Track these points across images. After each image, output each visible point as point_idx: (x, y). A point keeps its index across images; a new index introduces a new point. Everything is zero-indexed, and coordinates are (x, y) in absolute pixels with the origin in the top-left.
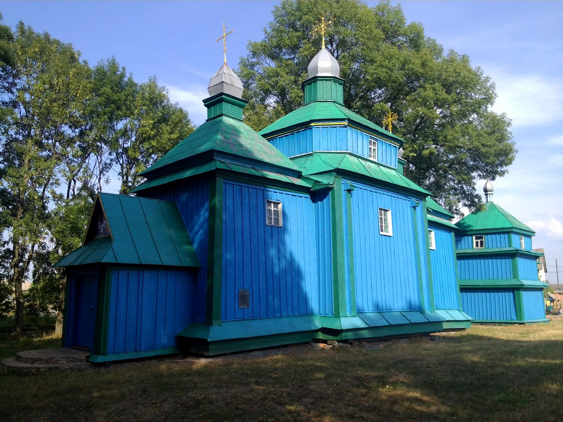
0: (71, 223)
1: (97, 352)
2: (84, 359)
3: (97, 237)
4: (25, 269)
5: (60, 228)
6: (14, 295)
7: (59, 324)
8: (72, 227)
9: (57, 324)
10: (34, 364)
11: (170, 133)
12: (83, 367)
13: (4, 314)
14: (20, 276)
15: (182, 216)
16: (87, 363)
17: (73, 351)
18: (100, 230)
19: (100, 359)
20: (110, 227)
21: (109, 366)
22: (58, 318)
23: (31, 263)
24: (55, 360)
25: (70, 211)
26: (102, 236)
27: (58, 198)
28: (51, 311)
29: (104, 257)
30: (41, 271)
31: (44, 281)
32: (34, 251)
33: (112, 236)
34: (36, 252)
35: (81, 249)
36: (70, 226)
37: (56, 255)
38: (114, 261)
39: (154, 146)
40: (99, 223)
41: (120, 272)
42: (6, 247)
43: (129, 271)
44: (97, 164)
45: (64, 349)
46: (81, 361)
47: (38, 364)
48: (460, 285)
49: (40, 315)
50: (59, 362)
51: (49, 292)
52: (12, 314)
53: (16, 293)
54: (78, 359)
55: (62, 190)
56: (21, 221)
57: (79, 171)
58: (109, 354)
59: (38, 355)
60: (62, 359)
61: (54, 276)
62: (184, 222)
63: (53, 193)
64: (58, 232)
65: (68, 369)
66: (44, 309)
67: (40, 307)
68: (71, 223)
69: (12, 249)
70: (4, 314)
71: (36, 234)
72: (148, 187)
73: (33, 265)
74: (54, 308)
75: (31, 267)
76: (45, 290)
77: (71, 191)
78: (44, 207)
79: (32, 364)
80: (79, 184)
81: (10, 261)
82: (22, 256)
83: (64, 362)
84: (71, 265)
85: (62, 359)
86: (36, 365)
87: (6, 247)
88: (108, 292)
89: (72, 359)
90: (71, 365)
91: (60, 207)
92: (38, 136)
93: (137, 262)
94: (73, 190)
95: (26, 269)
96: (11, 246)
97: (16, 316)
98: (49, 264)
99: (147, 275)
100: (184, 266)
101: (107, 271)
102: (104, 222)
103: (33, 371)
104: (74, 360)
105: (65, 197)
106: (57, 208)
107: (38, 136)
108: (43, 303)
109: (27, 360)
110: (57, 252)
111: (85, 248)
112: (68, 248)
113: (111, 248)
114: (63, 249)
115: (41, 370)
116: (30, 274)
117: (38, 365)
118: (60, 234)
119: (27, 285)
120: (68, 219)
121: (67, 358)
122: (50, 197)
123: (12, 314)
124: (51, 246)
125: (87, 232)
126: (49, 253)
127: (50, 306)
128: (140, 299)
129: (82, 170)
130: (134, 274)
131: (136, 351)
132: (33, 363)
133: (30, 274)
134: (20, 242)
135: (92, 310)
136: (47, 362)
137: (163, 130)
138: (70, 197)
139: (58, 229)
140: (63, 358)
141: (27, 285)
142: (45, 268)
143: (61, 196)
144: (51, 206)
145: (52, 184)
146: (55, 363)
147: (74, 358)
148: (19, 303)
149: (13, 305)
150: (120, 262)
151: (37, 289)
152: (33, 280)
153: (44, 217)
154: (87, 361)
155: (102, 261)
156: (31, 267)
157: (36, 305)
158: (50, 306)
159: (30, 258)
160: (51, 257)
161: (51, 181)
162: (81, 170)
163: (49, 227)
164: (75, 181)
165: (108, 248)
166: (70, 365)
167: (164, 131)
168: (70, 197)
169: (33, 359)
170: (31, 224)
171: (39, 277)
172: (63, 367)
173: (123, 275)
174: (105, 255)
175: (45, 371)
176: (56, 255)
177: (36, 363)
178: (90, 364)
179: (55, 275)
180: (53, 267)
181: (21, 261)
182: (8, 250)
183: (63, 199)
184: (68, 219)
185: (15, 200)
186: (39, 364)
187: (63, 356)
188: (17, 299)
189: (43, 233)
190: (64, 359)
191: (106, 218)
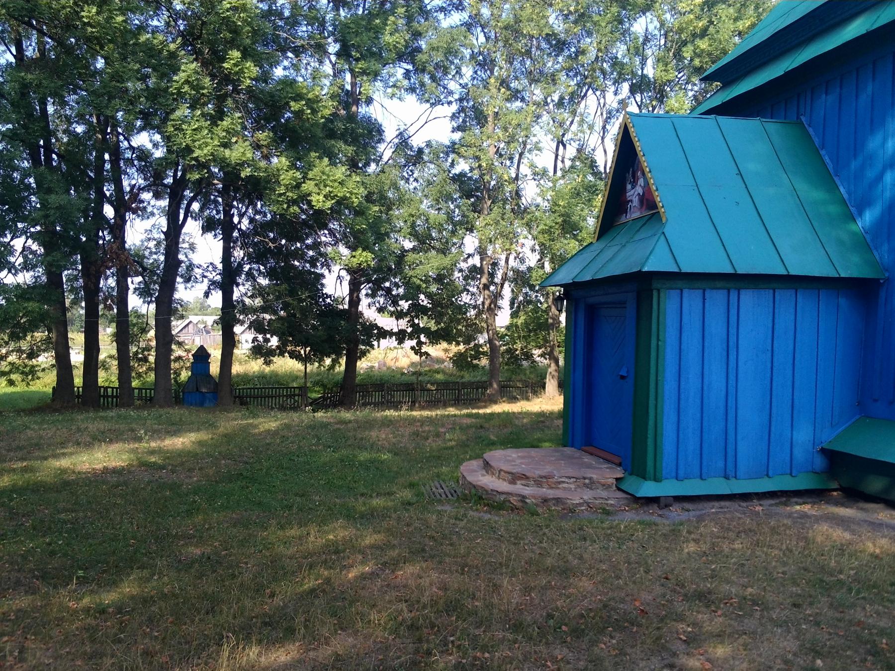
0: (562, 215)
1: (643, 475)
2: (613, 484)
3: (623, 219)
4: (498, 295)
5: (545, 225)
6: (486, 335)
7: (552, 381)
8: (564, 221)
9: (547, 380)
10: (515, 483)
11: (736, 20)
12: (612, 502)
13: (475, 362)
14: (493, 308)
15: (823, 152)
16: (620, 495)
17: (587, 459)
18: (631, 201)
19: (648, 489)
20: (657, 190)
21: (667, 506)
22: (550, 370)
23: (506, 285)
24: (554, 480)
25: (559, 195)
26: (636, 215)
27: (539, 174)
28: (538, 359)
29: (648, 258)
30: (521, 298)
31: (526, 313)
32: (510, 267)
33: (663, 210)
34: (513, 269)
35: (592, 248)
36: (560, 220)
37: (541, 272)
38: (673, 268)
39: (703, 51)
40: (629, 187)
41: (708, 294)
42: (471, 262)
43: (704, 291)
44: (599, 108)
45: (568, 450)
46: (607, 487)
47: (522, 485)
48: (625, 308)
49: (522, 365)
50: (560, 486)
51: (535, 330)
52: (484, 362)
53: (488, 333)
54: (598, 482)
55: (545, 160)
56: (488, 218)
57: (572, 123)
58: (666, 479)
59: (522, 463)
60: (567, 480)
61: (539, 305)
62: (830, 167)
63: (532, 166)
64: (543, 232)
65: (580, 505)
66: (528, 356)
67: (523, 354)
68: (562, 215)
69: (479, 265)
70: (475, 362)
71: (511, 238)
72: (728, 99)
73: (510, 289)
74: (542, 355)
75: (507, 292)
76: (527, 328)
77: (560, 165)
78: (518, 194)
79: (511, 483)
80: (571, 151)
81: (477, 283)
82: (492, 275)
83: (572, 486)
84: (576, 280)
85: (567, 480)
86: (519, 488)
87: (471, 262)
88: (658, 340)
89: (587, 481)
90: (588, 495)
91: (544, 189)
92: (500, 58)
93: (728, 270)
94: (563, 161)
95: (500, 295)
96: (476, 261)
97: (490, 365)
98: (532, 287)
99: (748, 298)
100: (843, 275)
101: (655, 294)
102: (641, 182)
103: (513, 499)
104: (591, 485)
105: (551, 173)
106: (539, 192)
107: (500, 58)
108: (526, 347)
109: (502, 473)
110: (543, 267)
111: (598, 246)
112: (560, 261)
113: (662, 238)
114: (552, 261)
115: (528, 501)
116: (505, 303)
117: (522, 487)
118: (546, 236)
119: (503, 319)
120: (557, 208)
121: (577, 478)
122: (529, 175)
123: (484, 362)
124: (532, 259)
125: (601, 217)
126: (530, 269)
127: (536, 352)
128: (732, 357)
129: (577, 119)
130: (717, 298)
131: (727, 477)
132: (513, 482)
133: (505, 303)
134: (489, 253)
135: (623, 377)
136: (538, 483)
137: (721, 17)
138: (559, 173)
139: (541, 227)
140: (570, 478)
141: (503, 319)
142: (526, 293)
143: (545, 172)
144: (530, 192)
145: (530, 151)
146: (553, 486)
147: (590, 479)
148: (493, 348)
149: (486, 349)
150: (685, 269)
151: (517, 326)
152: (510, 312)
153: (520, 212)
154: (619, 489)
155: (646, 269)
156: (507, 292)
157: (517, 350)
158: (536, 352)
159: (504, 279)
160: (534, 274)
161: (528, 147)
162: (575, 121)
163: (528, 225)
164: (564, 146)
165: (657, 237)
166: (585, 497)
167: (723, 18)
168: (559, 173)
169: (512, 473)
170: (501, 222)
171: (519, 307)
172: (571, 500)
173: (692, 298)
174: (651, 253)
175: (537, 505)
176: (541, 272)
177: (519, 482)
178: (627, 498)
179: (541, 303)
180: (537, 292)
181: (492, 282)
182: (474, 266)
183: (548, 175)
184: (557, 208)
185: (477, 189)
186: (525, 485)
187: (571, 472)
188: (490, 341)
189: (522, 237)
190: (572, 480)
191: (648, 169)
